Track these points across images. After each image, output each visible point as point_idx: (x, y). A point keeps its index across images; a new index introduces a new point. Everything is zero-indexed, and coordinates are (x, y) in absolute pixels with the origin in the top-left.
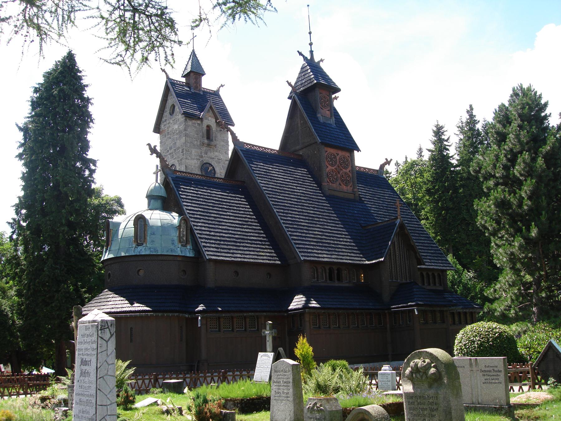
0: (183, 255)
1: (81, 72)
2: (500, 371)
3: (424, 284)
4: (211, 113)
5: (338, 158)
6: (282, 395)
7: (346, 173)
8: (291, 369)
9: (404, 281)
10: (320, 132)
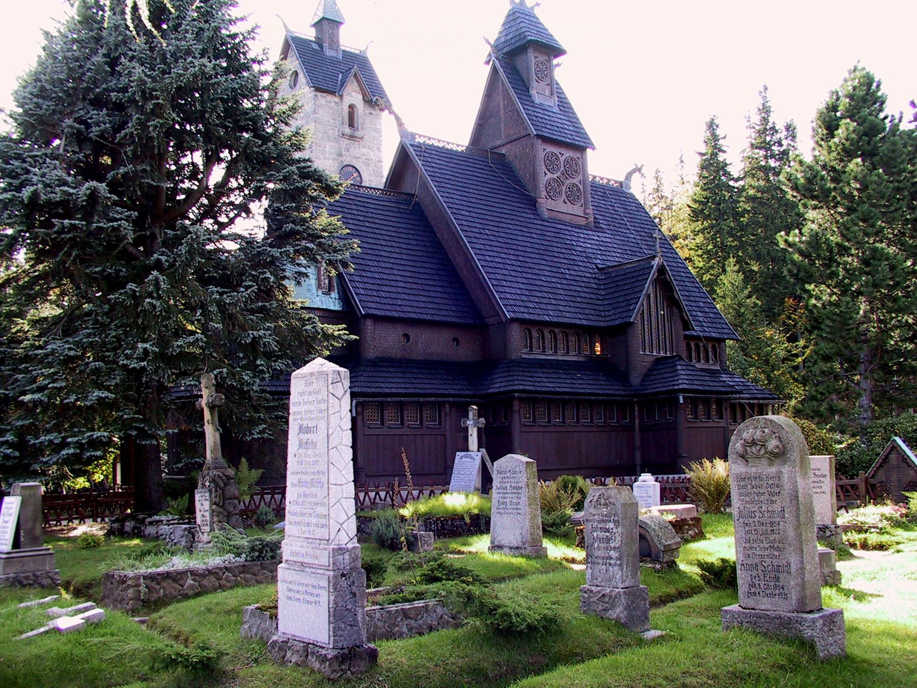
0: (325, 307)
1: (39, 57)
2: (824, 476)
3: (691, 360)
5: (562, 159)
6: (509, 506)
8: (523, 469)
9: (662, 354)
10: (535, 119)
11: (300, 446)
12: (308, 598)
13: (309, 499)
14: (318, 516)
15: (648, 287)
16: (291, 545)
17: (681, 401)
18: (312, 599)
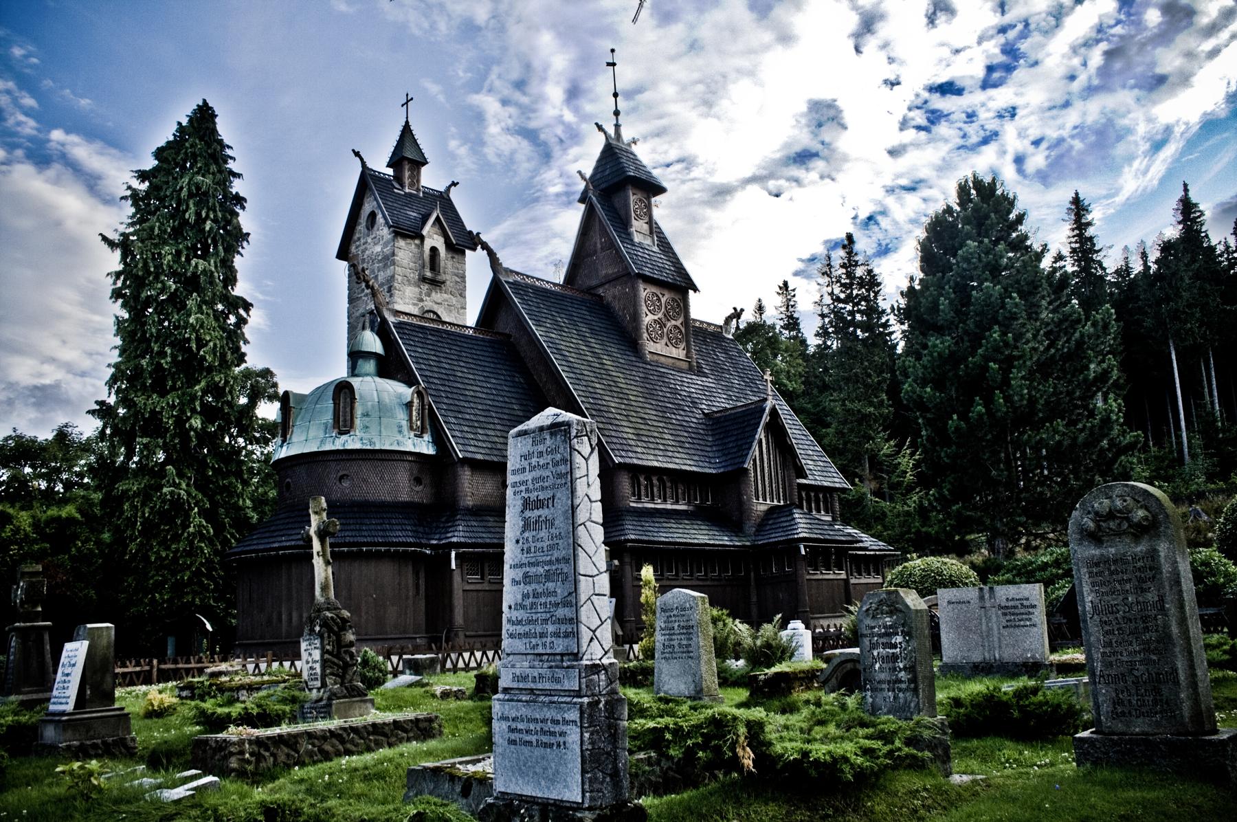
0: (417, 450)
4: (436, 229)
5: (663, 300)
7: (675, 327)
9: (776, 503)
11: (527, 526)
12: (545, 739)
13: (543, 600)
14: (561, 621)
15: (761, 434)
16: (513, 666)
17: (803, 552)
18: (553, 740)
